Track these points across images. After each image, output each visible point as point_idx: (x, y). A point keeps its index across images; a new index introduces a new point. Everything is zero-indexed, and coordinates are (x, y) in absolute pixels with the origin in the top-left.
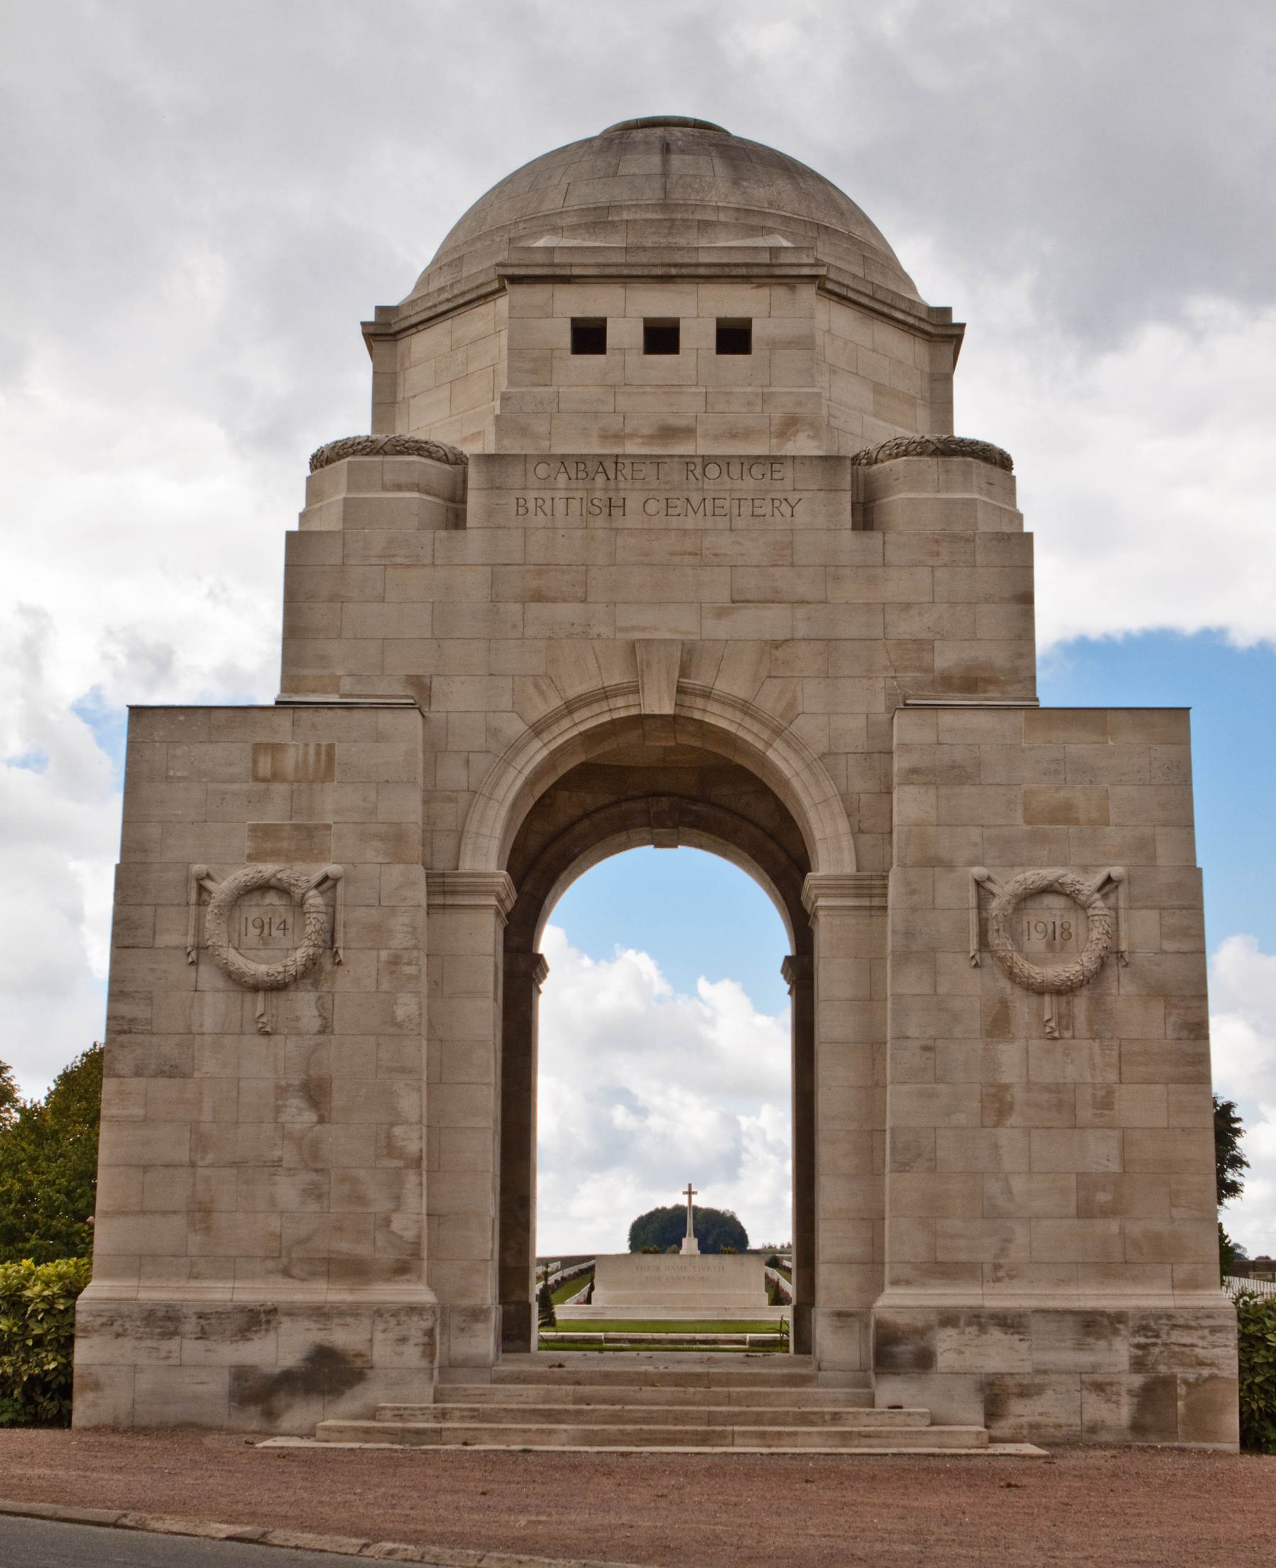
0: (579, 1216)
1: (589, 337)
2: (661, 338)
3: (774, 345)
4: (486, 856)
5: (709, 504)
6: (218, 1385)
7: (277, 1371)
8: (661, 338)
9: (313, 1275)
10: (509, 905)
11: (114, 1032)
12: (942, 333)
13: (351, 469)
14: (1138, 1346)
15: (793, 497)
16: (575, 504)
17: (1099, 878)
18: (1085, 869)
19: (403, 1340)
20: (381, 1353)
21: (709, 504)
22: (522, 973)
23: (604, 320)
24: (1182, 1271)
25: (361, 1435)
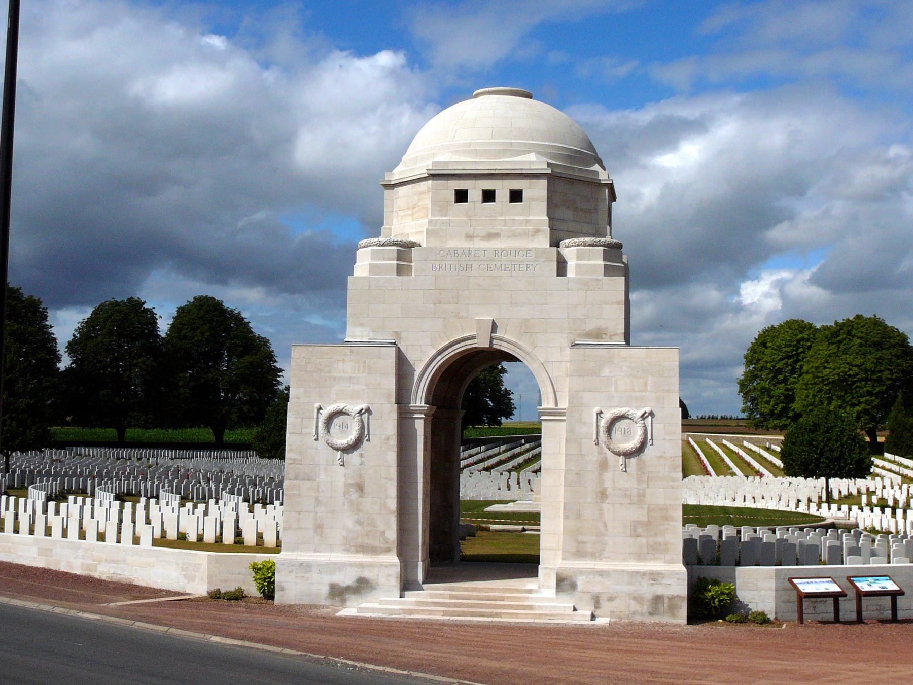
1: (461, 196)
2: (489, 196)
3: (531, 200)
6: (325, 589)
7: (345, 585)
9: (357, 552)
13: (373, 252)
15: (535, 264)
17: (641, 413)
18: (637, 408)
19: (389, 575)
20: (382, 580)
24: (668, 557)
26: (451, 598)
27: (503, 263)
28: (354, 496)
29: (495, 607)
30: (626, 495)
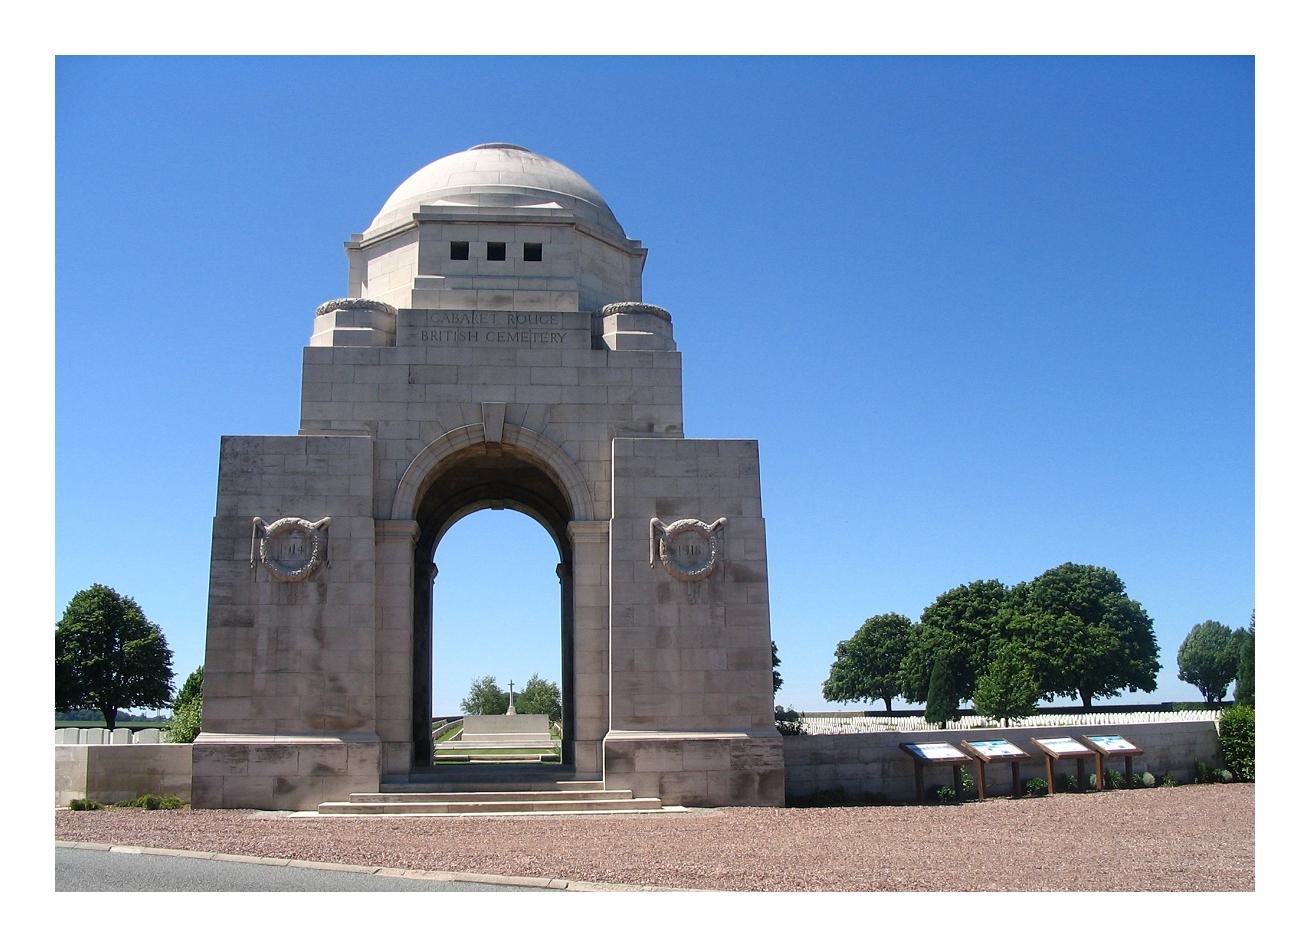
0: (448, 698)
2: (496, 252)
4: (406, 502)
5: (520, 336)
8: (496, 252)
10: (417, 539)
11: (226, 623)
12: (636, 253)
14: (736, 757)
16: (452, 336)
19: (362, 761)
21: (520, 336)
22: (424, 573)
23: (468, 244)
25: (342, 811)
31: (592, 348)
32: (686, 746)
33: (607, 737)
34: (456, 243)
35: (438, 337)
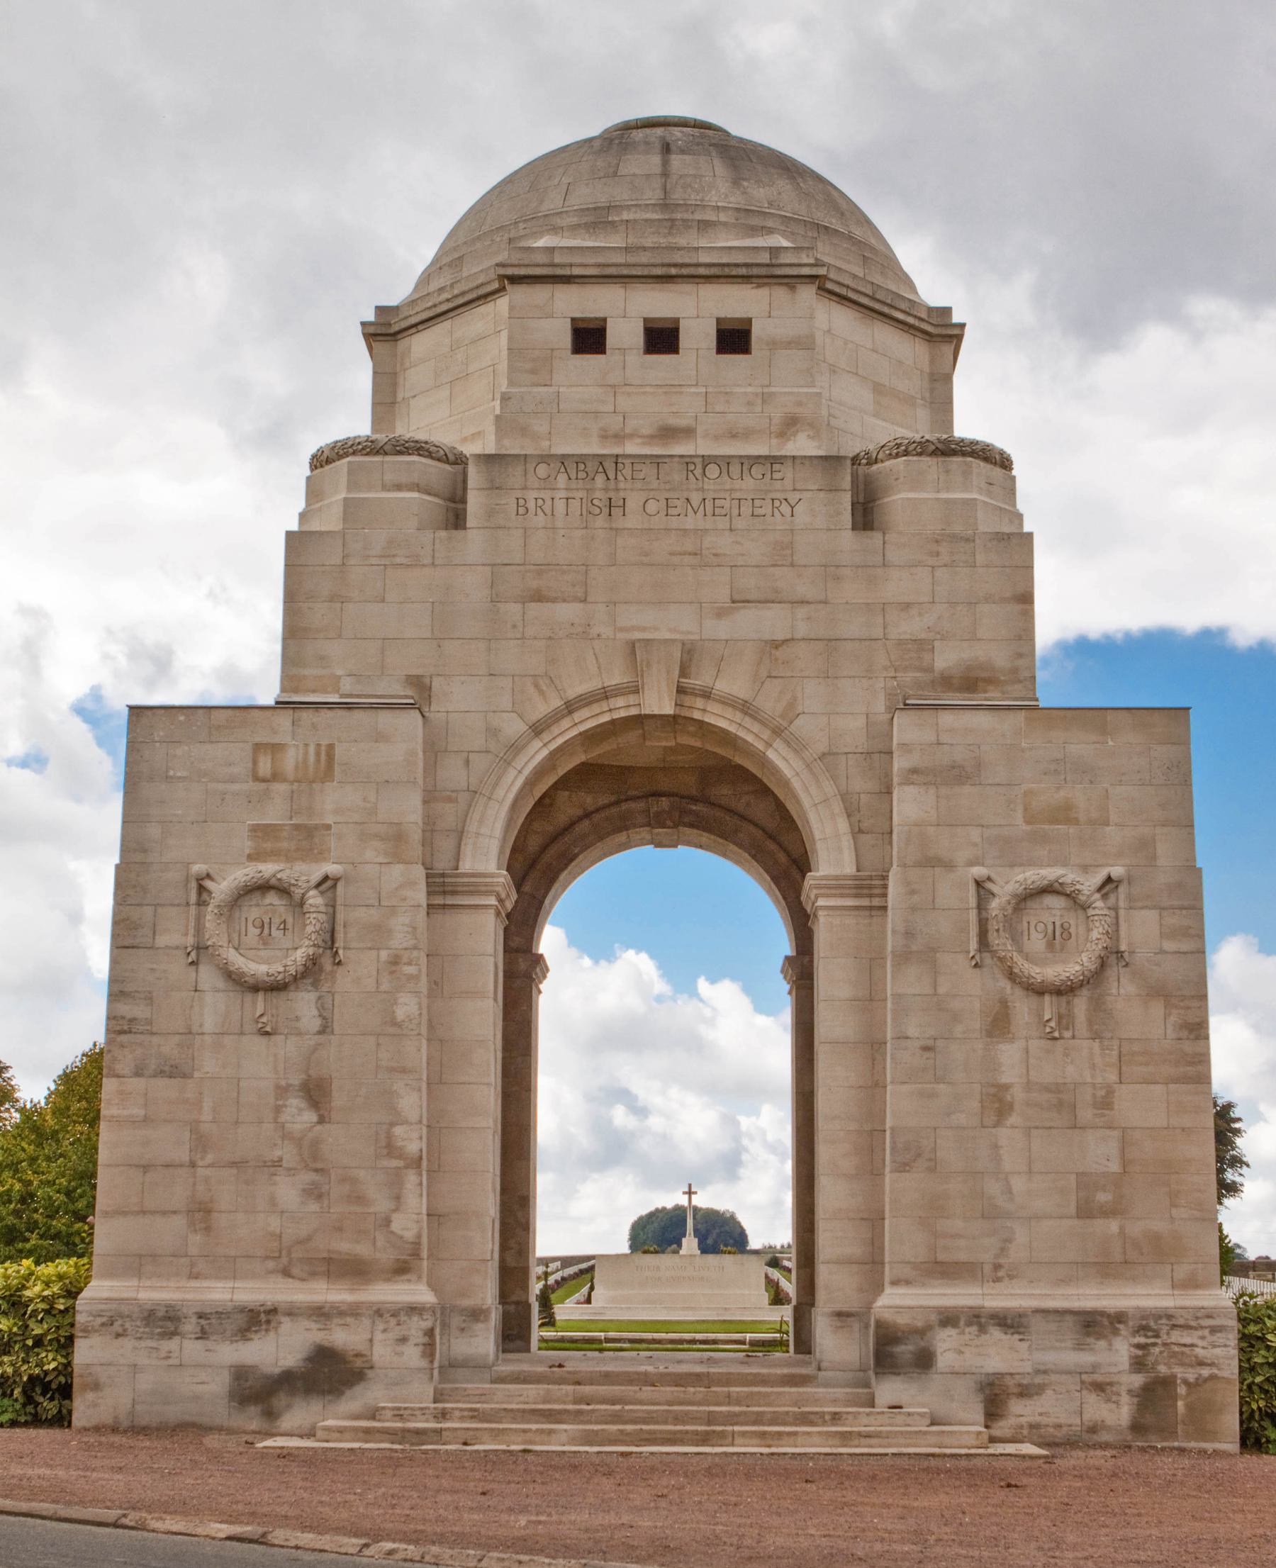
5: (709, 504)
6: (218, 1385)
7: (277, 1371)
8: (662, 338)
9: (313, 1275)
10: (509, 906)
11: (115, 1032)
12: (941, 333)
14: (1138, 1346)
15: (793, 497)
16: (575, 504)
18: (1085, 868)
19: (403, 1340)
20: (382, 1353)
21: (709, 504)
22: (521, 974)
26: (767, 1395)
27: (710, 496)
28: (300, 1116)
29: (677, 1419)
30: (1061, 1104)
31: (853, 529)
32: (1037, 1323)
33: (881, 1302)
34: (725, 319)
35: (548, 511)
